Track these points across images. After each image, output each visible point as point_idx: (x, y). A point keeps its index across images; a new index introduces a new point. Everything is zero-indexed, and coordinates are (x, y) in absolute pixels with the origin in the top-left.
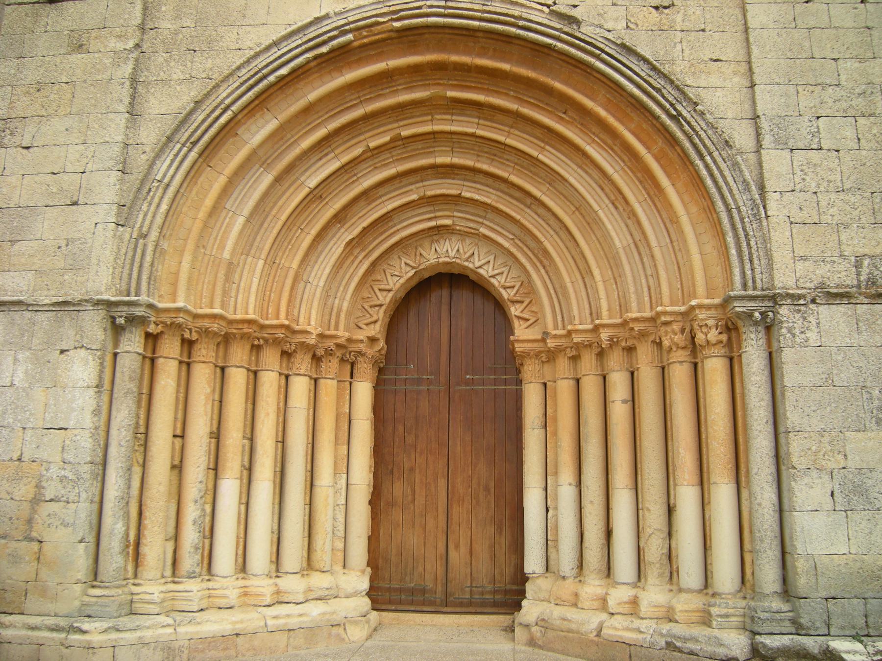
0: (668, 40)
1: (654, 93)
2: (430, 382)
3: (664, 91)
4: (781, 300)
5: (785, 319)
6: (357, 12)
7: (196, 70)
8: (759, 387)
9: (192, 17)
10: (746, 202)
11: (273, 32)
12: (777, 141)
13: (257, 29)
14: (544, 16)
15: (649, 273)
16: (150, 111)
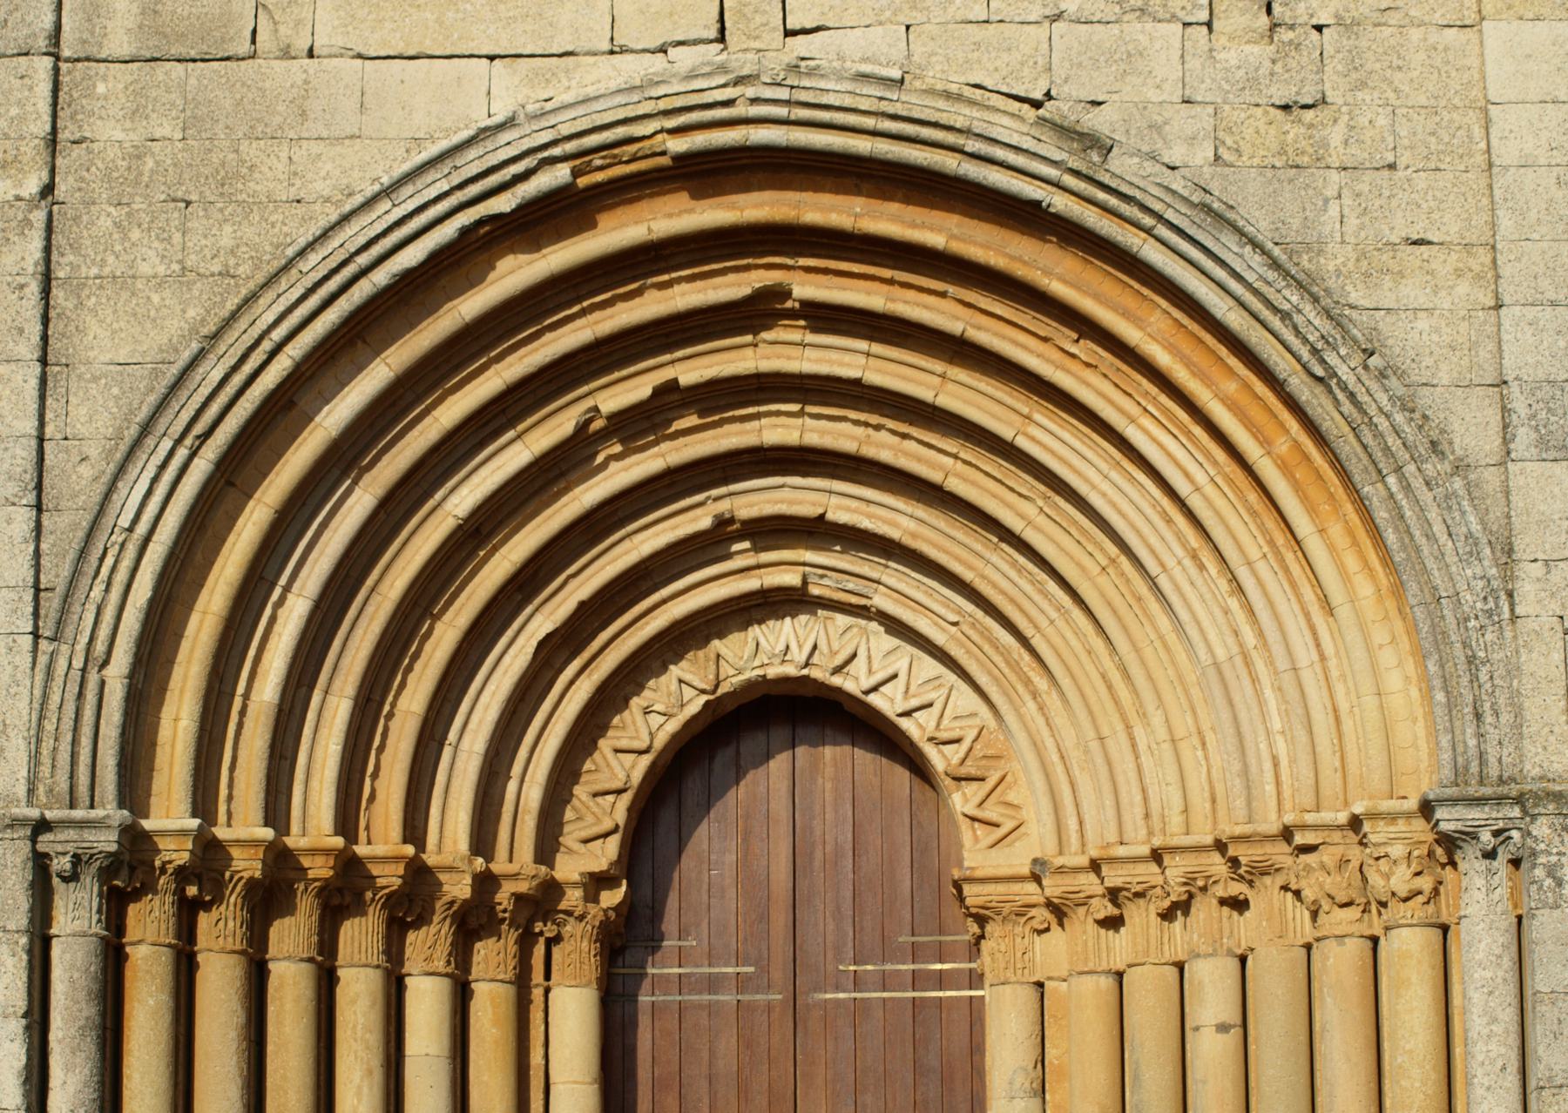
0: (1311, 192)
1: (1276, 322)
2: (741, 983)
3: (1298, 319)
4: (1536, 805)
5: (1542, 846)
6: (580, 111)
7: (197, 253)
8: (1491, 993)
9: (174, 113)
10: (1473, 583)
11: (378, 157)
12: (1542, 443)
13: (339, 148)
14: (1025, 129)
15: (1277, 725)
16: (91, 354)
